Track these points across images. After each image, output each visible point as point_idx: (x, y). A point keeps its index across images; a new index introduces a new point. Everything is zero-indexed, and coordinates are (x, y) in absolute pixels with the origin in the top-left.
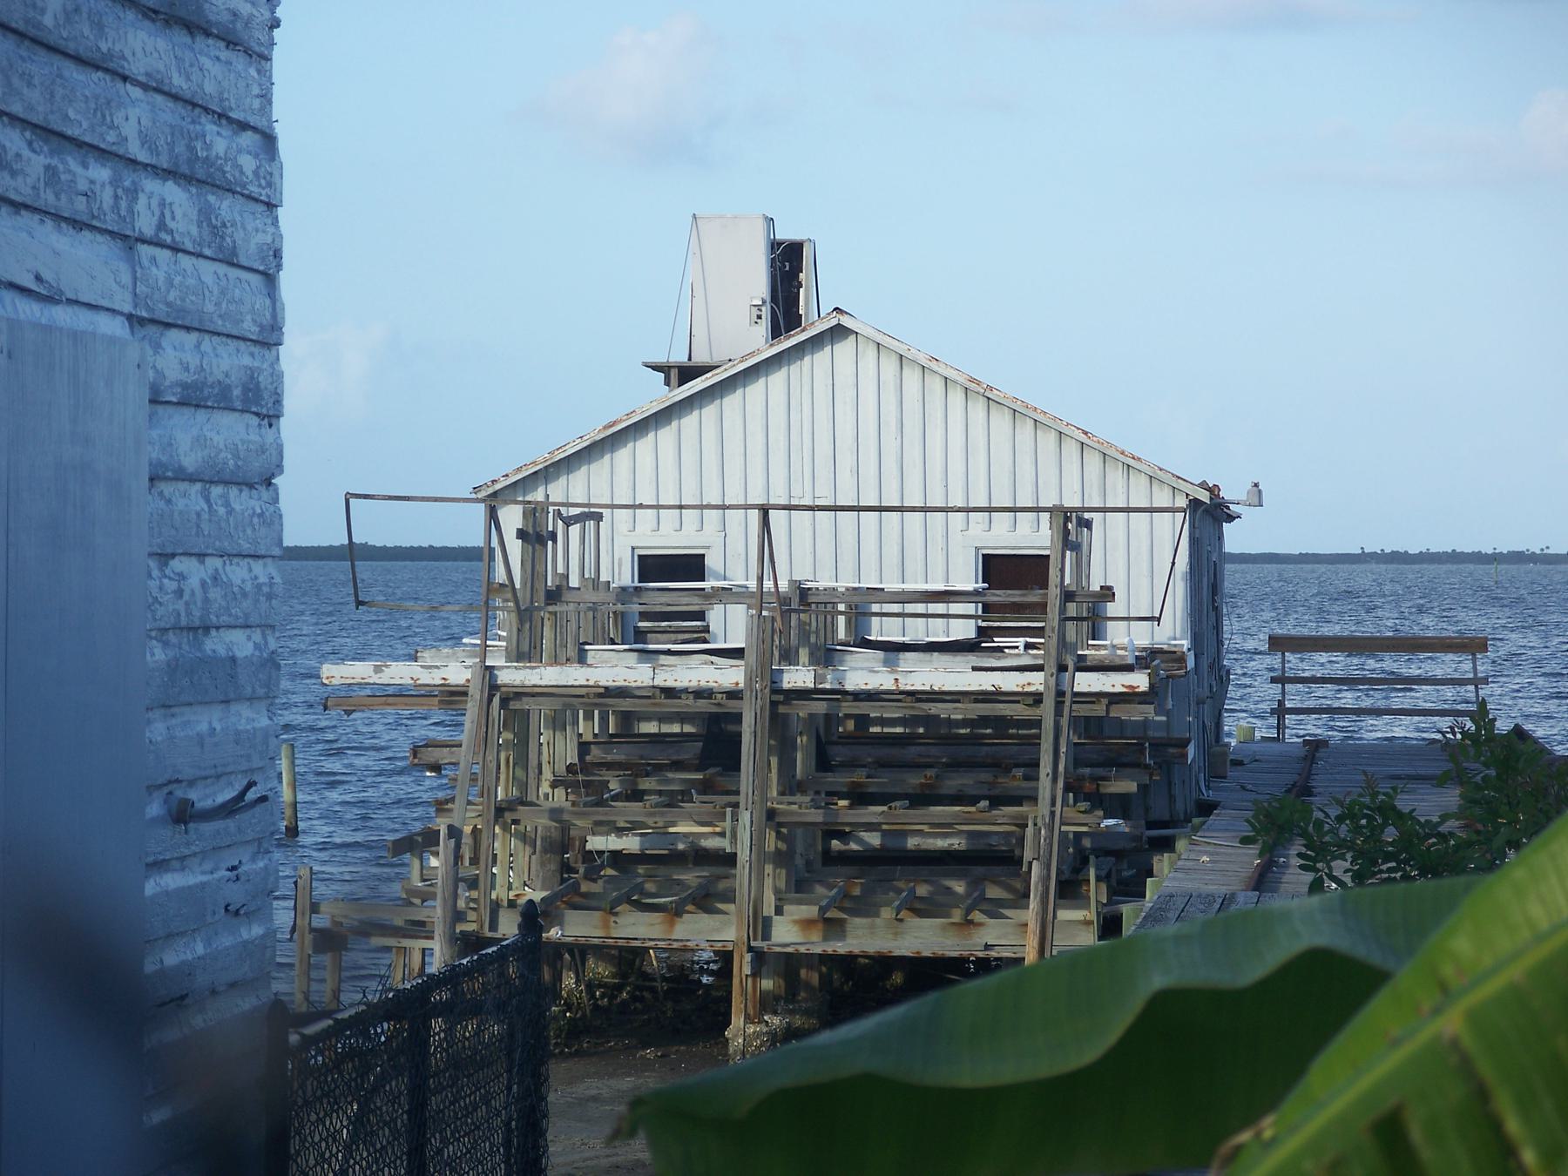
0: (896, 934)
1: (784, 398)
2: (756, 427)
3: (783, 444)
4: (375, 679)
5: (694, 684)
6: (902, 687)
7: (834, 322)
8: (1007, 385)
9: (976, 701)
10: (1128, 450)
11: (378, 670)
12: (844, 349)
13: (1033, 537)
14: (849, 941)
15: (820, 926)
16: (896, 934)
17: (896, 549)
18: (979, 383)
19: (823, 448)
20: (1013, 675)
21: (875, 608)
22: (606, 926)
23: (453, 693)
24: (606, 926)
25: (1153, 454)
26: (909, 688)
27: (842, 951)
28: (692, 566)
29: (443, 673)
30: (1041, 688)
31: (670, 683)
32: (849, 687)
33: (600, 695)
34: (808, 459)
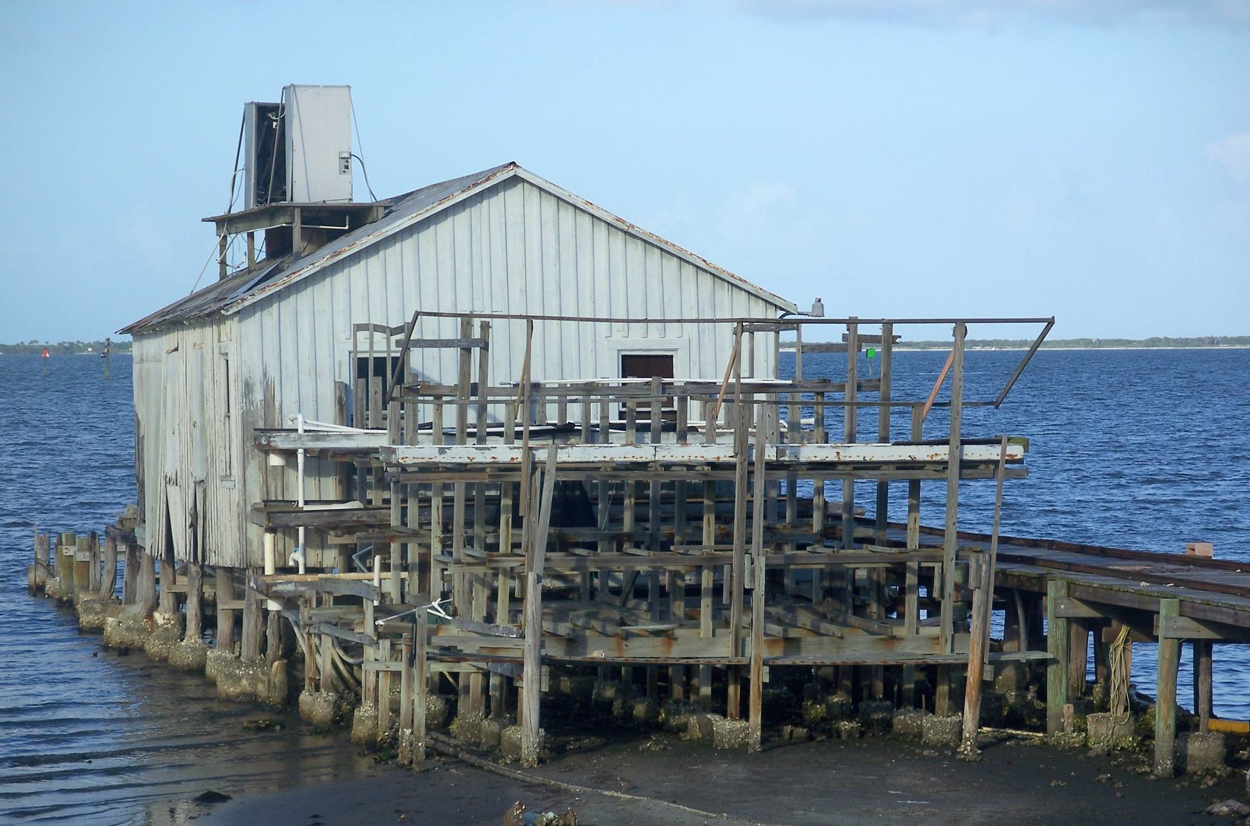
0: (838, 648)
1: (467, 233)
2: (445, 255)
3: (467, 271)
4: (440, 459)
5: (686, 459)
6: (842, 459)
7: (511, 174)
8: (644, 225)
9: (898, 468)
10: (736, 274)
11: (442, 451)
12: (514, 194)
13: (382, 346)
14: (803, 654)
15: (782, 644)
16: (838, 648)
17: (556, 353)
18: (623, 222)
19: (499, 272)
20: (532, 443)
21: (489, 398)
22: (620, 649)
23: (501, 470)
24: (620, 649)
25: (756, 280)
26: (847, 459)
27: (798, 662)
28: (660, 365)
29: (492, 453)
30: (946, 458)
31: (668, 459)
32: (803, 459)
33: (614, 469)
34: (486, 279)
